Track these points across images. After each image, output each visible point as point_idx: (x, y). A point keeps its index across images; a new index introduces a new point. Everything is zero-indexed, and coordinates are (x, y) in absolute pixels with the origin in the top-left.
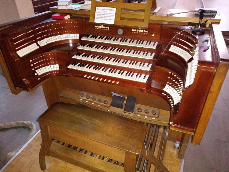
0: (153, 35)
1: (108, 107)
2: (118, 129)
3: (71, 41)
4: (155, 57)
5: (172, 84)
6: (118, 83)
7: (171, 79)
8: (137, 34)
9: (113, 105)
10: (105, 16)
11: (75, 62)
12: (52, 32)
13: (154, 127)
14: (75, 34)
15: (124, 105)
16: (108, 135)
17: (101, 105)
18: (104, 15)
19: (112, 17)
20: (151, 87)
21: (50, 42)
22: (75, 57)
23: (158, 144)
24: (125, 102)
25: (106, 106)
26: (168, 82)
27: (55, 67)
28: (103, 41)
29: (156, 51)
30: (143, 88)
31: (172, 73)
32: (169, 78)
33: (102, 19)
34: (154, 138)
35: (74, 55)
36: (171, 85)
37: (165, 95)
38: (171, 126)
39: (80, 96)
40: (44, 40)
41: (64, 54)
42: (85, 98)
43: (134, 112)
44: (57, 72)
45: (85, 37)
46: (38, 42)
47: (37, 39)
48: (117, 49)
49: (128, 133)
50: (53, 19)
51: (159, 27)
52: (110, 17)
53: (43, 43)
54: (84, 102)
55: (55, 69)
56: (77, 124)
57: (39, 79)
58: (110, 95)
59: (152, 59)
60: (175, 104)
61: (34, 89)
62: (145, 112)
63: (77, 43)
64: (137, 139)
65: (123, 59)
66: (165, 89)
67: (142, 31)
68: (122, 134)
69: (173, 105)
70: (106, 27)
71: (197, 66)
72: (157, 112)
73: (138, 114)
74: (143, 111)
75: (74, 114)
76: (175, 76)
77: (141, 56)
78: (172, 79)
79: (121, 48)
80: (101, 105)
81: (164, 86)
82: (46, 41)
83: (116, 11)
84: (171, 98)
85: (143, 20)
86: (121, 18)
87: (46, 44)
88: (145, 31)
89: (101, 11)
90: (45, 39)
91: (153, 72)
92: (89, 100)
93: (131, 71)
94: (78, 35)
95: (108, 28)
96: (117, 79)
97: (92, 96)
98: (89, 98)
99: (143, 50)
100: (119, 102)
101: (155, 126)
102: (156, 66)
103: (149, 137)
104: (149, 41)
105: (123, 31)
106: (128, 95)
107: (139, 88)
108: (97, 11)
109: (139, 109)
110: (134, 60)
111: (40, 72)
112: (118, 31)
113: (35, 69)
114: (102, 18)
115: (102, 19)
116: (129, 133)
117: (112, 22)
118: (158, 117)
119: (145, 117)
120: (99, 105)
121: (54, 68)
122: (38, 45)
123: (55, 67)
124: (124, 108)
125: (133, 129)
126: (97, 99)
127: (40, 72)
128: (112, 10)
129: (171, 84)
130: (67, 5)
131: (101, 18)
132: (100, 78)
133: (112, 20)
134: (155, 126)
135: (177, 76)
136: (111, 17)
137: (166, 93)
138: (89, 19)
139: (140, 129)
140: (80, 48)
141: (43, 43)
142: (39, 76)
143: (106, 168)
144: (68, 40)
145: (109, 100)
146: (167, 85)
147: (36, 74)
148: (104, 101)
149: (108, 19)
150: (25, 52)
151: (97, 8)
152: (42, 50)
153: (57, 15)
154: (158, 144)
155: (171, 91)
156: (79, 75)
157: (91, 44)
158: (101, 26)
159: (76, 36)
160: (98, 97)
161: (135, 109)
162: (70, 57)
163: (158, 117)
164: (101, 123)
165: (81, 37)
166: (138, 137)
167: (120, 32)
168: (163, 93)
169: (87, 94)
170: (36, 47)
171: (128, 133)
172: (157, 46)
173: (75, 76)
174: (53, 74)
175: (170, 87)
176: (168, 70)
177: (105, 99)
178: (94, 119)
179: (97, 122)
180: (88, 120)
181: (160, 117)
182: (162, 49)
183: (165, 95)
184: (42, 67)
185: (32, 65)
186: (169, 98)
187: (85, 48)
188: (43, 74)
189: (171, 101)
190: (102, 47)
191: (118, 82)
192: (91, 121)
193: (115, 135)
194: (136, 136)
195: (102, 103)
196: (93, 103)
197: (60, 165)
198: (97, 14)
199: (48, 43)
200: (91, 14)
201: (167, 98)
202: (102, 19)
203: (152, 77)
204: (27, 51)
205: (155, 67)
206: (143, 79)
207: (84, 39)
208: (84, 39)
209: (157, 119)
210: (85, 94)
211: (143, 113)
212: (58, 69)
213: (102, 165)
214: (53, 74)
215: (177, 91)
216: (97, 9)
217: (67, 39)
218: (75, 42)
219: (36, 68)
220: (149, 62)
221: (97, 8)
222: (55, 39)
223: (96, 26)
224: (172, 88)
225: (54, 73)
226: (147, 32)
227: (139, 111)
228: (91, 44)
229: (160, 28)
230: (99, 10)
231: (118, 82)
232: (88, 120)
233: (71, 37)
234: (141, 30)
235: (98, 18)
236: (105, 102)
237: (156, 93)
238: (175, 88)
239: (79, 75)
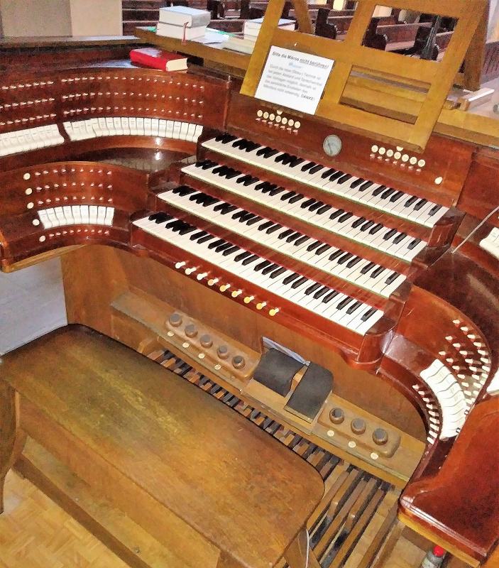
0: (438, 180)
1: (242, 379)
2: (223, 464)
3: (158, 142)
4: (425, 257)
5: (455, 364)
6: (273, 312)
7: (455, 345)
8: (384, 164)
9: (258, 377)
10: (292, 83)
11: (163, 213)
12: (109, 101)
13: (368, 484)
14: (192, 126)
15: (293, 387)
16: (183, 477)
17: (224, 367)
18: (290, 79)
19: (314, 89)
20: (380, 355)
21: (106, 133)
22: (169, 197)
23: (367, 540)
24: (298, 377)
25: (236, 376)
26: (443, 353)
27: (103, 216)
28: (367, 198)
29: (435, 236)
30: (352, 351)
31: (462, 325)
32: (449, 338)
33: (279, 90)
34: (357, 520)
35: (166, 190)
36: (449, 366)
37: (422, 393)
38: (404, 511)
39: (170, 327)
40: (86, 121)
41: (135, 183)
42: (182, 333)
43: (317, 417)
45: (217, 140)
46: (67, 125)
47: (66, 113)
48: (354, 218)
49: (252, 488)
50: (132, 64)
51: (465, 155)
52: (306, 89)
53: (81, 131)
54: (176, 345)
55: (101, 222)
56: (103, 411)
57: (42, 239)
58: (258, 345)
59: (411, 260)
60: (441, 438)
61: (18, 264)
62: (353, 430)
63: (187, 156)
64: (273, 517)
65: (337, 247)
66: (425, 375)
67: (285, 121)
68: (232, 485)
69: (435, 435)
70: (291, 122)
72: (392, 439)
73: (329, 428)
74: (347, 423)
75: (106, 376)
76: (472, 337)
77: (376, 241)
78: (457, 345)
79: (318, 201)
80: (224, 367)
81: (425, 362)
82: (96, 127)
83: (331, 71)
84: (438, 410)
85: (410, 120)
86: (342, 98)
87: (92, 136)
88: (413, 160)
89: (284, 63)
90: (93, 121)
91: (401, 304)
92: (194, 342)
93: (326, 285)
94: (199, 130)
95: (298, 125)
96: (274, 300)
97: (203, 331)
98: (195, 335)
99: (391, 222)
100: (281, 373)
101: (372, 483)
102: (415, 289)
103: (342, 514)
104: (418, 201)
106: (302, 356)
107: (339, 346)
108: (272, 60)
109: (334, 413)
110: (348, 252)
111: (51, 218)
112: (327, 143)
113: (37, 208)
114: (281, 88)
115: (282, 91)
116: (257, 490)
117: (310, 108)
118: (391, 456)
120: (218, 367)
122: (63, 132)
123: (103, 216)
124: (289, 396)
125: (276, 480)
126: (216, 346)
127: (51, 218)
128: (318, 65)
129: (450, 360)
130: (185, 26)
131: (278, 87)
132: (224, 282)
133: (311, 98)
134: (372, 483)
135: (477, 340)
136: (309, 87)
137: (425, 387)
138: (237, 83)
139: (299, 486)
140: (192, 171)
141: (81, 131)
142: (46, 233)
145: (252, 362)
146: (437, 364)
147: (36, 222)
148: (235, 356)
149: (300, 93)
150: (12, 145)
151: (274, 49)
152: (71, 151)
153: (152, 53)
154: (367, 540)
155: (445, 385)
156: (164, 256)
157: (229, 169)
158: (276, 115)
159: (190, 132)
160: (220, 341)
161: (322, 409)
162: (152, 193)
163: (391, 456)
164: (181, 427)
165: (204, 138)
166: (280, 513)
167: (333, 145)
168: (416, 387)
169: (191, 323)
170: (54, 137)
171: (252, 488)
172: (443, 218)
173: (151, 256)
174: (83, 234)
175: (446, 371)
176: (453, 311)
177: (239, 353)
178: (162, 409)
179: (169, 423)
180: (141, 408)
181: (398, 458)
182: (458, 234)
183: (422, 393)
184: (62, 204)
185: (29, 191)
186: (430, 407)
187: (208, 176)
188: (60, 229)
189: (435, 421)
190: (333, 210)
191: (277, 310)
192: (148, 413)
193: (207, 482)
194: (276, 510)
196: (201, 356)
197: (46, 515)
198: (270, 72)
199: (99, 134)
200: (251, 67)
201: (422, 408)
202: (279, 90)
203: (394, 322)
204: (19, 144)
205: (413, 290)
206: (358, 322)
207: (212, 145)
208: (212, 145)
209: (385, 461)
210: (187, 320)
211: (348, 429)
212: (109, 222)
214: (86, 234)
215: (465, 392)
216: (274, 54)
217: (148, 133)
218: (178, 152)
219: (41, 203)
220: (400, 267)
221: (274, 49)
222: (123, 126)
223: (260, 113)
224: (452, 379)
225: (89, 234)
226: (422, 163)
228: (229, 169)
229: (470, 161)
230: (279, 58)
231: (277, 310)
232: (141, 408)
233: (160, 130)
234: (403, 153)
235: (269, 85)
236: (236, 360)
237: (394, 379)
238: (459, 381)
239: (164, 256)
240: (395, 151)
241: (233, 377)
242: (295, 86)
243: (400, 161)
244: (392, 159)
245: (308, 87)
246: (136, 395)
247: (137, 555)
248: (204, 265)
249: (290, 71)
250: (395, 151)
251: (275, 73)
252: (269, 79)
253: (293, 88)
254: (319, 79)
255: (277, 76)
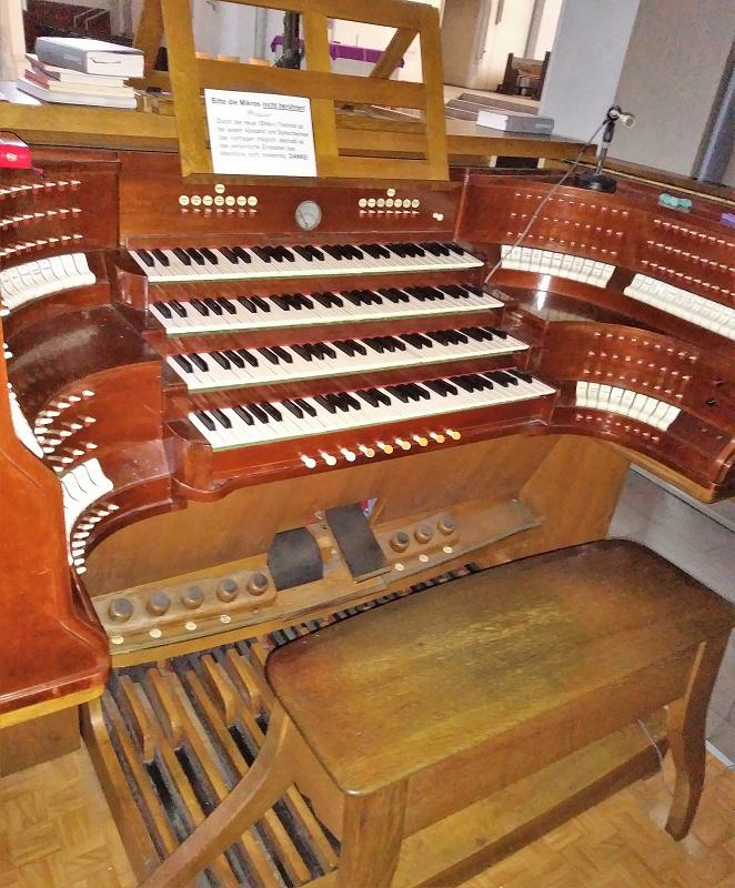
18: (260, 135)
19: (302, 142)
44: (632, 429)
52: (292, 145)
67: (230, 201)
71: (545, 319)
89: (240, 112)
95: (253, 201)
105: (318, 203)
119: (222, 619)
121: (631, 407)
131: (247, 151)
143: (520, 811)
144: (532, 277)
151: (210, 94)
167: (309, 215)
195: (243, 600)
213: (497, 813)
221: (210, 94)
222: (574, 267)
223: (184, 200)
227: (114, 609)
240: (214, 195)
241: (256, 612)
242: (274, 144)
243: (225, 207)
244: (213, 207)
245: (294, 141)
246: (478, 630)
247: (487, 844)
248: (330, 441)
249: (254, 124)
250: (214, 195)
251: (230, 130)
252: (224, 142)
253: (272, 148)
254: (301, 127)
255: (237, 134)
